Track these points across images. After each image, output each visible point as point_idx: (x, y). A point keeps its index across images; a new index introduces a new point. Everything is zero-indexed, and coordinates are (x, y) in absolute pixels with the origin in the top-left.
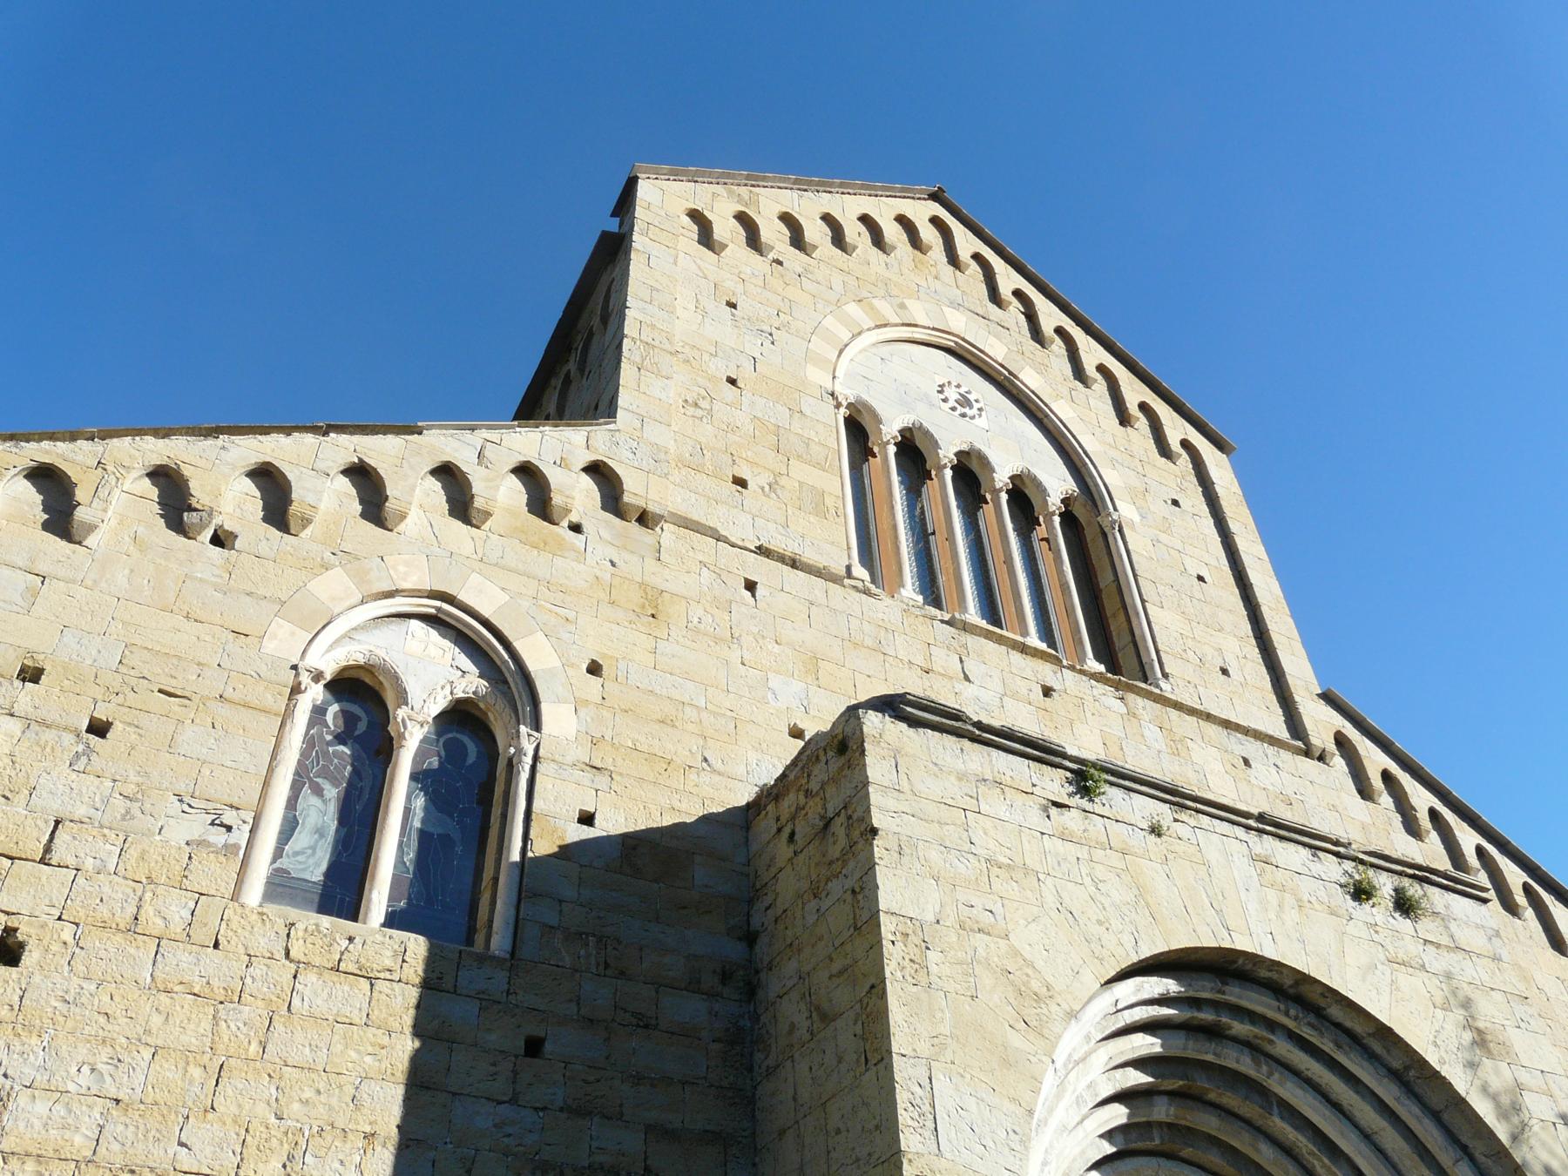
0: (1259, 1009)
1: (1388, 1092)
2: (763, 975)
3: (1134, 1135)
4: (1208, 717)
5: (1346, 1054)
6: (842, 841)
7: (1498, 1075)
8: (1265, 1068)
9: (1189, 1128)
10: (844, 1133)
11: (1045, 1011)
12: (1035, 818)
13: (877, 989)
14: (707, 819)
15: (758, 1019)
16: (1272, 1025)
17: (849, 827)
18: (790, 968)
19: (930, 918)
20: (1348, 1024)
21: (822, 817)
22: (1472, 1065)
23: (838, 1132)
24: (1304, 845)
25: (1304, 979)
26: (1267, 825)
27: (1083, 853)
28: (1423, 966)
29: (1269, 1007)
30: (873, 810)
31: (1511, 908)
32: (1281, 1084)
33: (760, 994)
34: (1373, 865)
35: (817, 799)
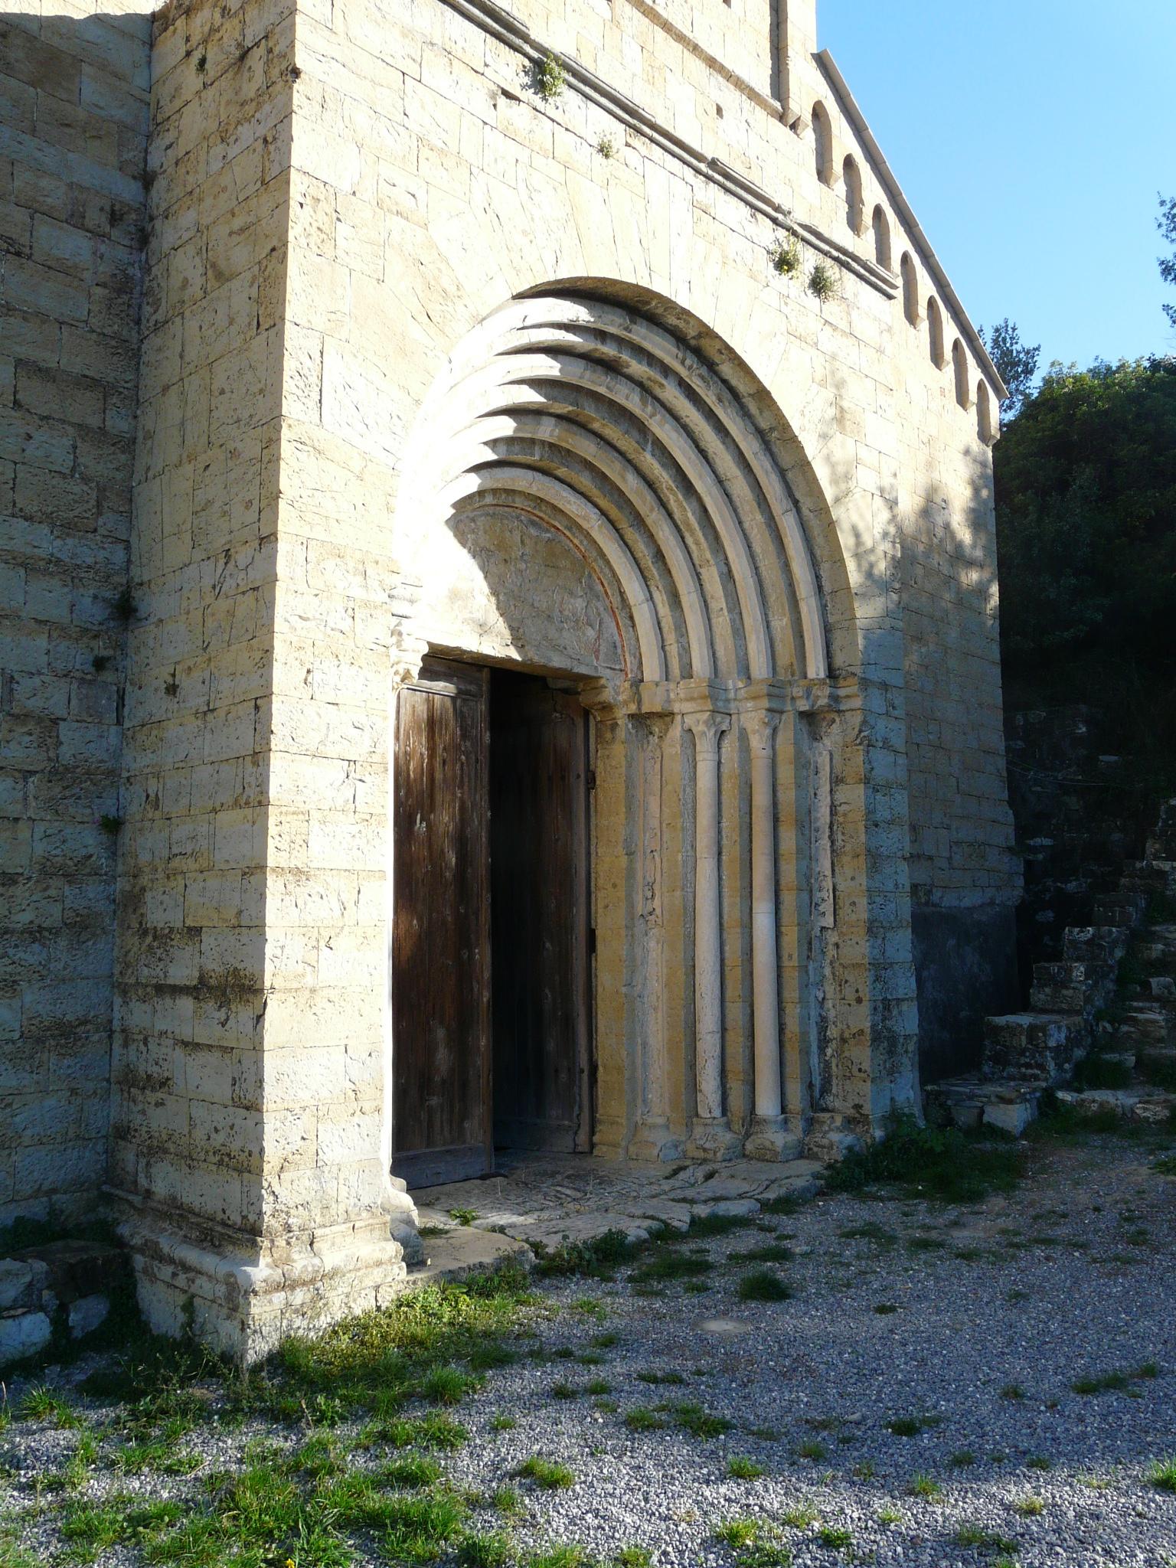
0: (658, 352)
1: (750, 446)
2: (158, 223)
3: (517, 448)
4: (695, 49)
5: (724, 407)
6: (259, 79)
7: (842, 448)
8: (649, 409)
9: (568, 451)
10: (228, 395)
11: (450, 309)
12: (481, 104)
13: (278, 252)
14: (98, 20)
15: (150, 269)
16: (666, 370)
17: (268, 63)
18: (187, 218)
19: (346, 187)
20: (734, 382)
21: (239, 45)
22: (824, 437)
23: (222, 392)
24: (747, 203)
25: (707, 332)
26: (718, 174)
27: (524, 155)
28: (816, 344)
29: (668, 352)
30: (298, 46)
31: (911, 316)
32: (661, 426)
33: (154, 243)
34: (804, 240)
35: (235, 21)
